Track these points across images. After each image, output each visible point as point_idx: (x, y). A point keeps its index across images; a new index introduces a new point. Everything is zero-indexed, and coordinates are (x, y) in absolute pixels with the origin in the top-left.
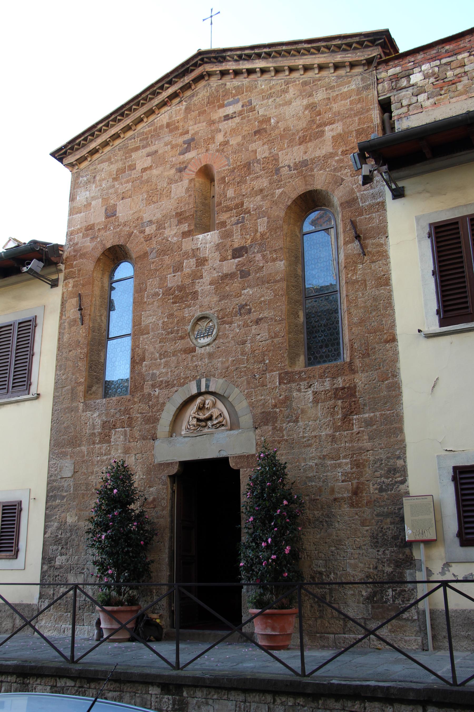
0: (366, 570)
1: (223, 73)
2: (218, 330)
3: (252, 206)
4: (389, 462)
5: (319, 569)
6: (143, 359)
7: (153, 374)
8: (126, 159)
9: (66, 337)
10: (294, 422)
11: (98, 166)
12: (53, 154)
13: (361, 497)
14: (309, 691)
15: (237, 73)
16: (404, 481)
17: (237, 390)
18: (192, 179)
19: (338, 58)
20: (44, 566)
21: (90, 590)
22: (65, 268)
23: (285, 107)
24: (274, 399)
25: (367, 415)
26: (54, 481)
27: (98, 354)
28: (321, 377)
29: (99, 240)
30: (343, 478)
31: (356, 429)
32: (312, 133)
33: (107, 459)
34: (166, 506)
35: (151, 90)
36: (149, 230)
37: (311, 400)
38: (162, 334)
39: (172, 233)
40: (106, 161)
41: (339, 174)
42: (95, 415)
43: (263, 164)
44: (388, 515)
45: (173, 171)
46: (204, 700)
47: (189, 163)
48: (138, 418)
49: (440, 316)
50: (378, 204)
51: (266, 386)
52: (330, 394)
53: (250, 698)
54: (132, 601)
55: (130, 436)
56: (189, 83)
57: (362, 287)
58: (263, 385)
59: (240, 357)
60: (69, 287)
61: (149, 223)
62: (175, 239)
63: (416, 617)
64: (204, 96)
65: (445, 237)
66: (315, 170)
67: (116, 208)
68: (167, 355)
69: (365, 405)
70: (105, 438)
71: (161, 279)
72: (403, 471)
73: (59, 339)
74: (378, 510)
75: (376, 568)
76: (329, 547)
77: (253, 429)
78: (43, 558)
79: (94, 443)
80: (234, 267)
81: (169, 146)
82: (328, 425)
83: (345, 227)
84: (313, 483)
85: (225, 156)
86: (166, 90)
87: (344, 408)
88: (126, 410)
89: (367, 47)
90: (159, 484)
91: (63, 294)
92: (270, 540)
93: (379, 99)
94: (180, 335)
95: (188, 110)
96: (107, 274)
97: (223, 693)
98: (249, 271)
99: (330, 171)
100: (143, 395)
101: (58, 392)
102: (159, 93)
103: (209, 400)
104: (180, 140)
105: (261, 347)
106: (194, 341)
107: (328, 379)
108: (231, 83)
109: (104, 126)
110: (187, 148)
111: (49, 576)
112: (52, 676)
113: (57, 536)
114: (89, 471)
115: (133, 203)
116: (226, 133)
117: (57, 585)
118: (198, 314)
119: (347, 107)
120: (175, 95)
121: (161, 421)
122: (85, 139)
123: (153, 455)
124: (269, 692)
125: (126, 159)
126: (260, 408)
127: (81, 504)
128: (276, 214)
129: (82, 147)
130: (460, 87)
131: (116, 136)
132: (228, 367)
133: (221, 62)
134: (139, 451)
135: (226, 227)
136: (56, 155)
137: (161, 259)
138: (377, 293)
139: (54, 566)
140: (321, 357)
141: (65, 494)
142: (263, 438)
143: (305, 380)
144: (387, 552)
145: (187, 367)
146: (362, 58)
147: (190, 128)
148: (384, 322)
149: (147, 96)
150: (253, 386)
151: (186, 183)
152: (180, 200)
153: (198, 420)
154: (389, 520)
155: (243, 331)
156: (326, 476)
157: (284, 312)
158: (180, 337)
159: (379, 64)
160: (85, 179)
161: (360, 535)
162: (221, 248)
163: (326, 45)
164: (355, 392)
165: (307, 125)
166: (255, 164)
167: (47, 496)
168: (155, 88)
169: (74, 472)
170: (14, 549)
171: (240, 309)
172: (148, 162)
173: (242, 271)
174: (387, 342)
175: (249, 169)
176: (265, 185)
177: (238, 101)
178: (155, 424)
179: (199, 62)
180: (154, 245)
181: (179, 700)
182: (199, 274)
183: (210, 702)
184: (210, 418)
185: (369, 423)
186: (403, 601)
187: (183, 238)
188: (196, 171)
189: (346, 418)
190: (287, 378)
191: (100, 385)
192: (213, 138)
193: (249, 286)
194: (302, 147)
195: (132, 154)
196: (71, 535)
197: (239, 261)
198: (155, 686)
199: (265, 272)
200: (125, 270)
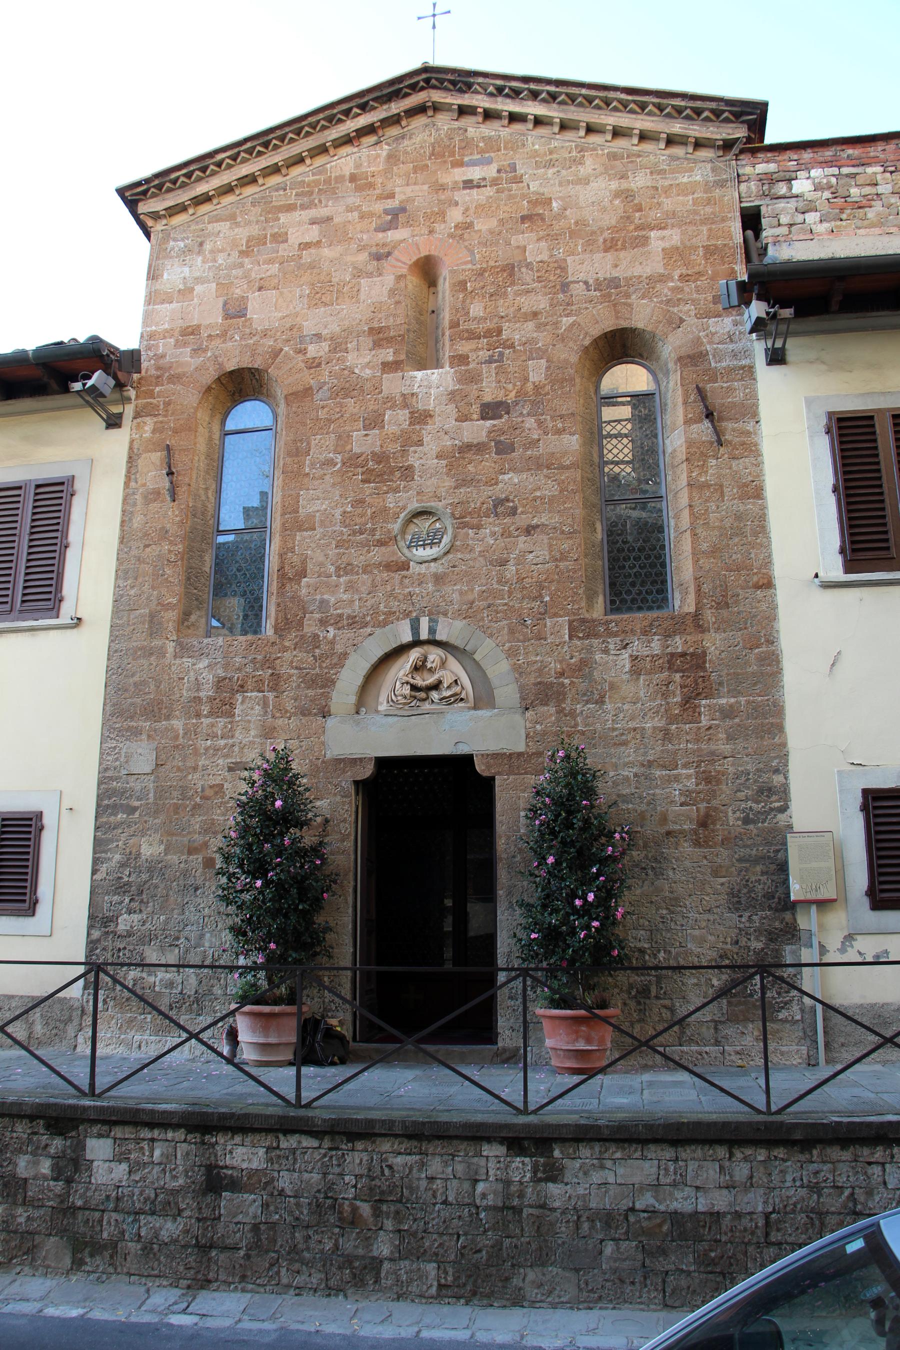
0: (720, 945)
1: (463, 111)
2: (455, 537)
3: (517, 337)
4: (760, 777)
5: (639, 945)
6: (303, 574)
7: (322, 601)
8: (267, 221)
9: (138, 521)
10: (596, 703)
11: (210, 227)
12: (121, 192)
13: (713, 831)
14: (798, 1136)
15: (489, 115)
16: (784, 809)
17: (489, 643)
18: (401, 276)
19: (677, 127)
20: (93, 932)
21: (193, 976)
22: (137, 397)
23: (578, 187)
24: (561, 662)
25: (723, 701)
26: (111, 778)
27: (201, 556)
28: (645, 633)
29: (209, 354)
30: (683, 799)
31: (705, 721)
32: (627, 236)
33: (226, 744)
34: (349, 834)
35: (328, 113)
36: (313, 350)
37: (627, 670)
38: (342, 533)
39: (362, 360)
40: (226, 220)
41: (675, 310)
42: (201, 665)
43: (538, 271)
44: (757, 860)
45: (363, 257)
46: (595, 1161)
47: (394, 247)
48: (291, 676)
49: (845, 557)
50: (743, 368)
51: (545, 639)
52: (661, 661)
53: (686, 1153)
54: (291, 1000)
55: (274, 707)
56: (398, 114)
57: (717, 495)
58: (540, 637)
59: (495, 586)
60: (146, 432)
61: (315, 338)
62: (368, 371)
63: (798, 1017)
64: (425, 141)
65: (851, 435)
66: (634, 297)
67: (246, 305)
68: (352, 570)
69: (721, 684)
70: (223, 706)
71: (339, 437)
72: (784, 792)
73: (123, 522)
74: (743, 852)
75: (737, 942)
76: (657, 909)
77: (520, 711)
78: (91, 917)
79: (198, 715)
80: (484, 434)
81: (356, 214)
82: (657, 712)
83: (686, 395)
84: (630, 806)
85: (466, 247)
86: (354, 117)
87: (686, 687)
88: (266, 660)
89: (727, 120)
90: (335, 795)
91: (132, 442)
92: (591, 897)
93: (743, 205)
94: (377, 537)
95: (392, 158)
96: (218, 417)
97: (633, 1149)
98: (513, 444)
99: (661, 302)
100: (302, 637)
101: (120, 618)
102: (340, 121)
103: (434, 655)
104: (379, 207)
105: (535, 574)
106: (406, 551)
107: (656, 638)
108: (474, 128)
109: (228, 157)
110: (391, 222)
111: (104, 949)
112: (268, 1131)
113: (121, 878)
114: (189, 764)
115: (280, 300)
116: (467, 210)
117: (122, 965)
118: (414, 505)
119: (688, 208)
120: (370, 130)
121: (339, 685)
122: (189, 175)
123: (323, 743)
124: (720, 1142)
125: (267, 221)
126: (533, 675)
127: (171, 822)
128: (563, 357)
129: (180, 187)
130: (871, 214)
131: (250, 180)
132: (472, 603)
133: (461, 91)
134: (294, 735)
135: (468, 364)
136: (127, 194)
137: (340, 403)
138: (742, 508)
139: (115, 933)
140: (633, 601)
141: (137, 804)
142: (538, 727)
143: (616, 636)
144: (754, 917)
145: (391, 595)
146: (718, 137)
147: (397, 190)
148: (752, 556)
149: (318, 122)
150: (521, 638)
151: (389, 280)
152: (377, 308)
153: (414, 688)
154: (758, 868)
155: (501, 543)
156: (654, 795)
157: (577, 520)
158: (378, 541)
159: (742, 151)
160: (182, 244)
161: (710, 891)
162: (457, 398)
163: (659, 104)
164: (705, 662)
165: (618, 222)
166: (524, 270)
167: (98, 805)
168: (335, 111)
169: (157, 765)
170: (27, 898)
171: (495, 506)
172: (313, 234)
173: (498, 443)
174: (758, 587)
175: (511, 275)
176: (542, 306)
177: (489, 162)
178: (327, 690)
179: (422, 84)
180: (325, 377)
181: (545, 1165)
182: (415, 438)
183: (609, 1164)
184: (436, 686)
185: (728, 713)
186: (779, 993)
187: (384, 371)
188: (410, 263)
189: (689, 702)
190: (582, 628)
191: (203, 613)
192: (442, 214)
193: (513, 469)
194: (609, 256)
195: (280, 215)
196: (151, 878)
197: (494, 426)
198: (494, 1144)
199: (542, 449)
200: (250, 414)
